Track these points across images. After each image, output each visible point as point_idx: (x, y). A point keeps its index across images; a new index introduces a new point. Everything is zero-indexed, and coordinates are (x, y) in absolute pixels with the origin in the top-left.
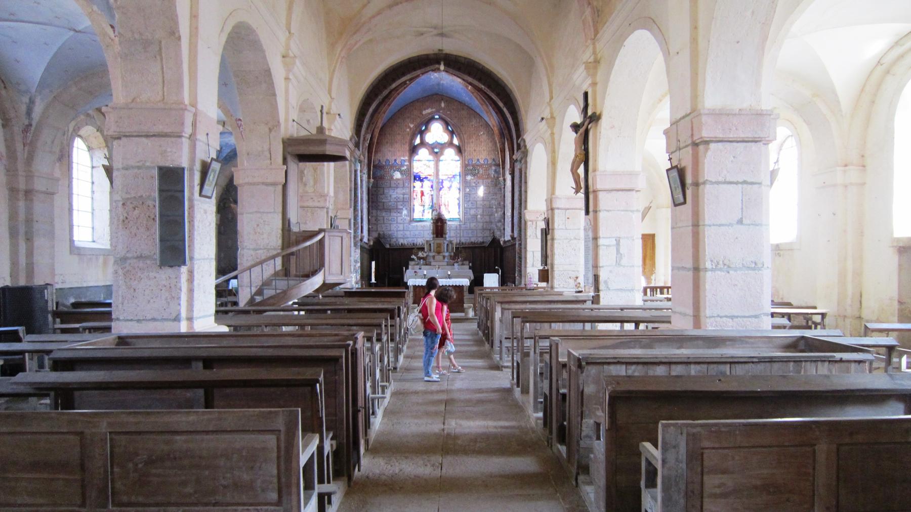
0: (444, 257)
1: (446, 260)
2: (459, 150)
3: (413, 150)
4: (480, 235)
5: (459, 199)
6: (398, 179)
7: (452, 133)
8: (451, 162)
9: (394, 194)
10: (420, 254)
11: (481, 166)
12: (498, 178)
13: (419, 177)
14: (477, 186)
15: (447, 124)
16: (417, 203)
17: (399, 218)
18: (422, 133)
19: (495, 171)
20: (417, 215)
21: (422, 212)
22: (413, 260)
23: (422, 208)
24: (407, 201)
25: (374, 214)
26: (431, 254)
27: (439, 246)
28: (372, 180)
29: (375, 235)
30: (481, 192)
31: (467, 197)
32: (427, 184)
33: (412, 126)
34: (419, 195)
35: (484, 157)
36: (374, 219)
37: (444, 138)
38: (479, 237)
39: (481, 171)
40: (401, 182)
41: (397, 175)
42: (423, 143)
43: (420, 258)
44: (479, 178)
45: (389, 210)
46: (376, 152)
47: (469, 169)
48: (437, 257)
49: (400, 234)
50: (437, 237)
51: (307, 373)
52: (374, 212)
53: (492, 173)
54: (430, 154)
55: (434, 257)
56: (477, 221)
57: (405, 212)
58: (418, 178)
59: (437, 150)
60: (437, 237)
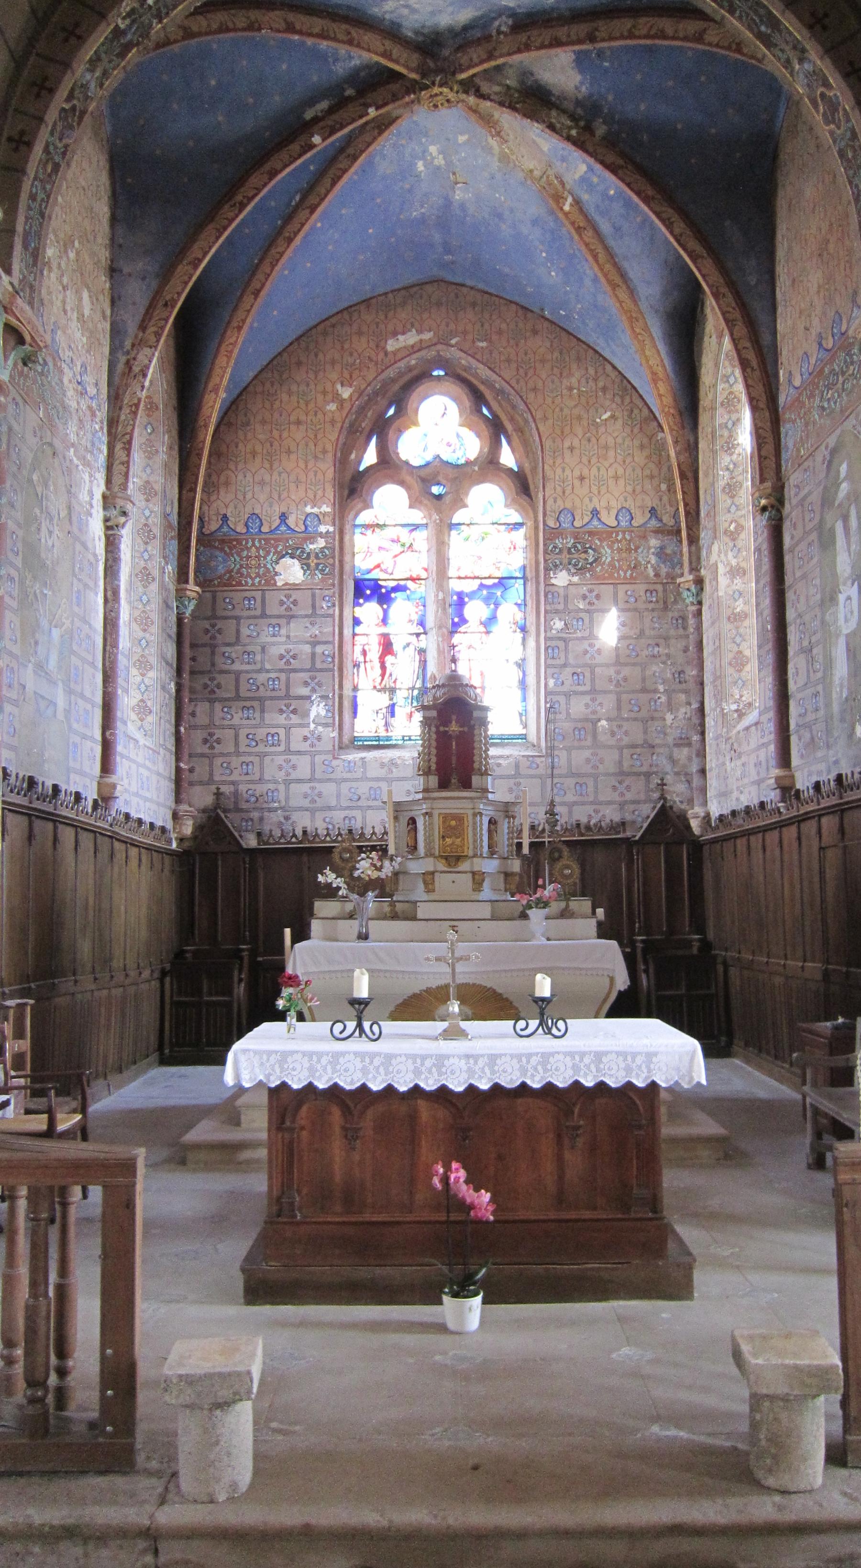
0: (478, 879)
1: (487, 893)
2: (522, 486)
3: (353, 488)
4: (607, 795)
5: (521, 665)
6: (295, 587)
7: (495, 430)
8: (491, 533)
9: (273, 645)
10: (364, 867)
11: (608, 534)
12: (672, 578)
13: (376, 586)
14: (593, 612)
15: (476, 396)
16: (366, 679)
17: (297, 734)
18: (383, 431)
19: (661, 553)
20: (366, 724)
21: (388, 717)
22: (330, 892)
23: (384, 700)
24: (331, 668)
25: (202, 719)
26: (416, 867)
27: (453, 826)
28: (193, 588)
29: (203, 798)
30: (609, 629)
31: (559, 650)
32: (402, 609)
33: (346, 393)
34: (374, 653)
35: (615, 505)
36: (199, 735)
37: (469, 445)
38: (607, 804)
39: (607, 554)
40: (303, 597)
41: (291, 571)
42: (389, 466)
43: (361, 887)
44: (600, 580)
45: (258, 702)
46: (211, 487)
47: (562, 547)
48: (443, 881)
49: (298, 794)
50: (444, 785)
51: (585, 780)
52: (202, 708)
53: (648, 557)
54: (414, 503)
55: (429, 879)
56: (596, 743)
57: (318, 710)
58: (369, 590)
59: (439, 489)
60: (444, 785)
